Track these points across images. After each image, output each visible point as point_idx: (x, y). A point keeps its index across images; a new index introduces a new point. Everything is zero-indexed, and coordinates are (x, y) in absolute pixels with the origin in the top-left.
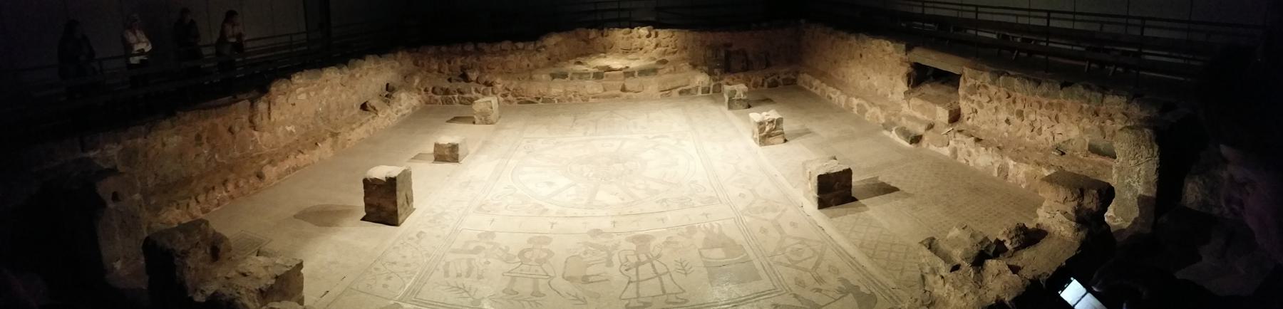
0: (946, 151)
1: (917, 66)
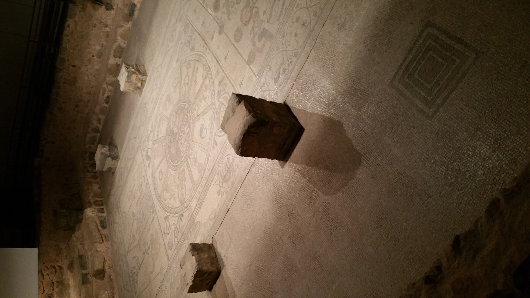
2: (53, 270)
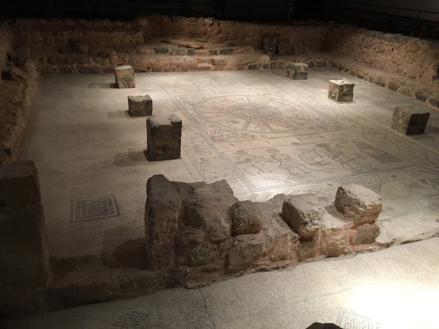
2: (235, 34)
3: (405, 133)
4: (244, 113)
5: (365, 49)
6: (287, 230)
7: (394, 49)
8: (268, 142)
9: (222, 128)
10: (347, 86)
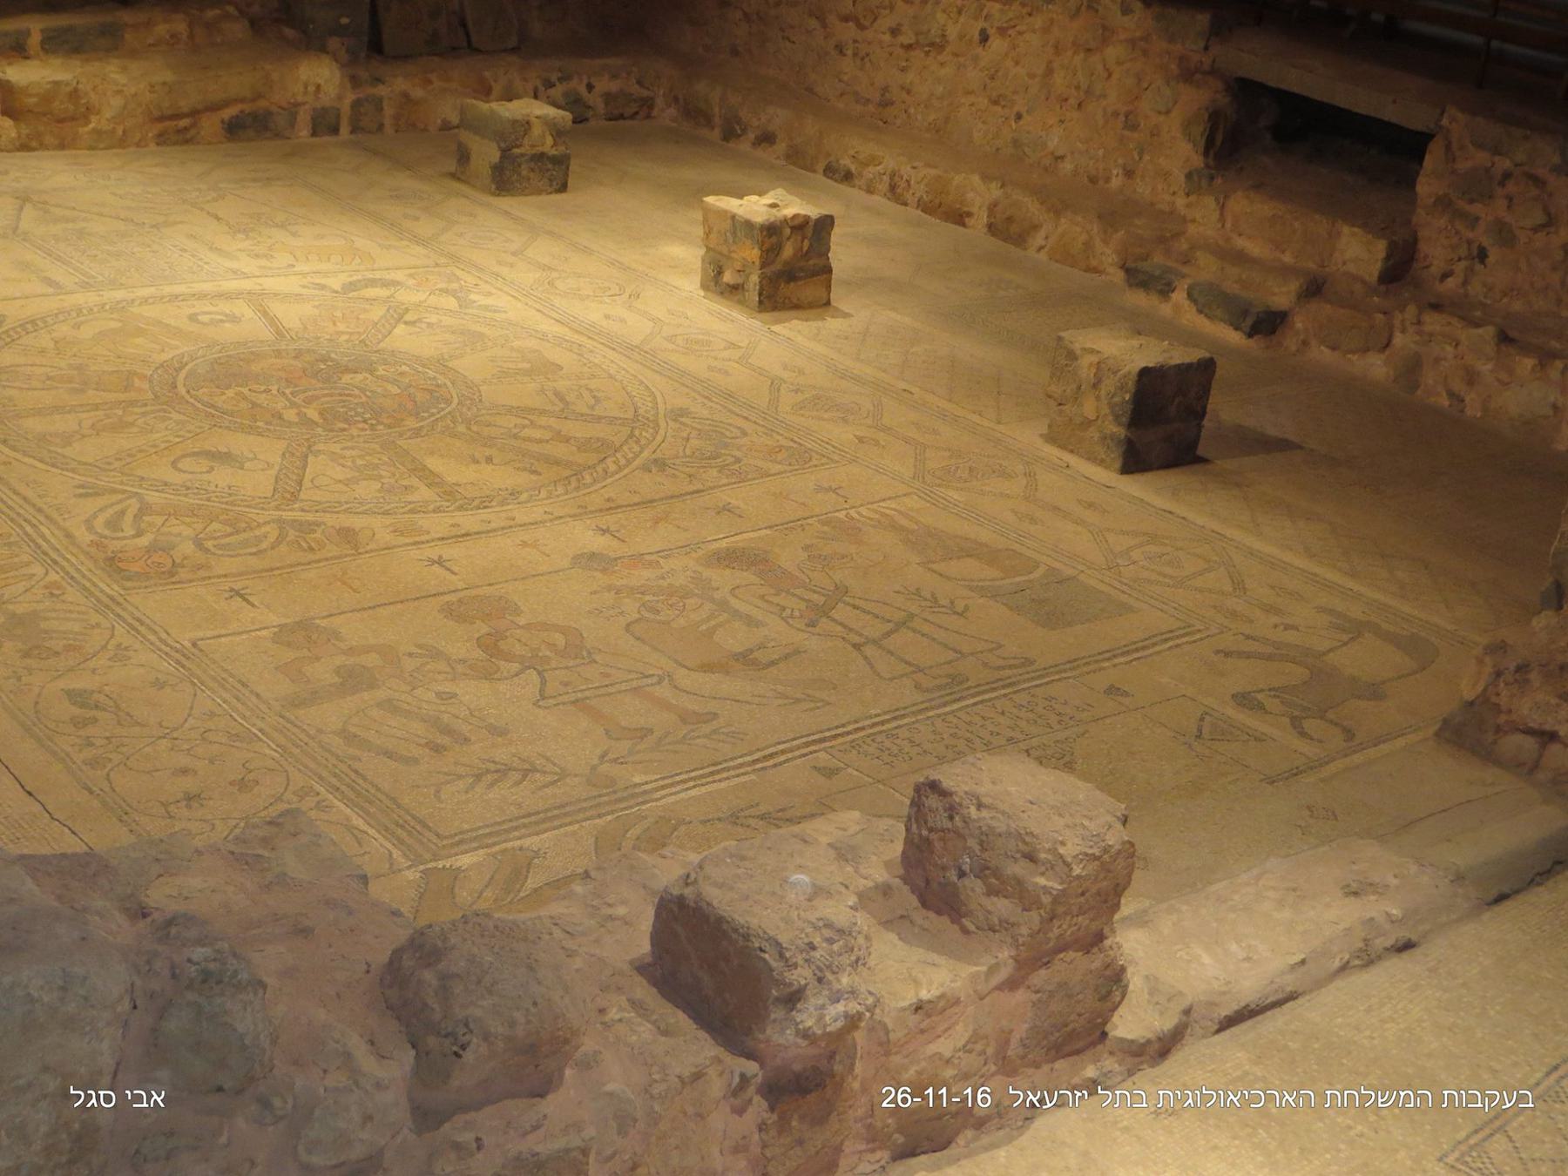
0: (1376, 367)
1: (1246, 90)
3: (1118, 464)
4: (262, 399)
5: (848, 32)
6: (696, 1049)
7: (991, 32)
8: (440, 562)
9: (153, 497)
10: (799, 226)
